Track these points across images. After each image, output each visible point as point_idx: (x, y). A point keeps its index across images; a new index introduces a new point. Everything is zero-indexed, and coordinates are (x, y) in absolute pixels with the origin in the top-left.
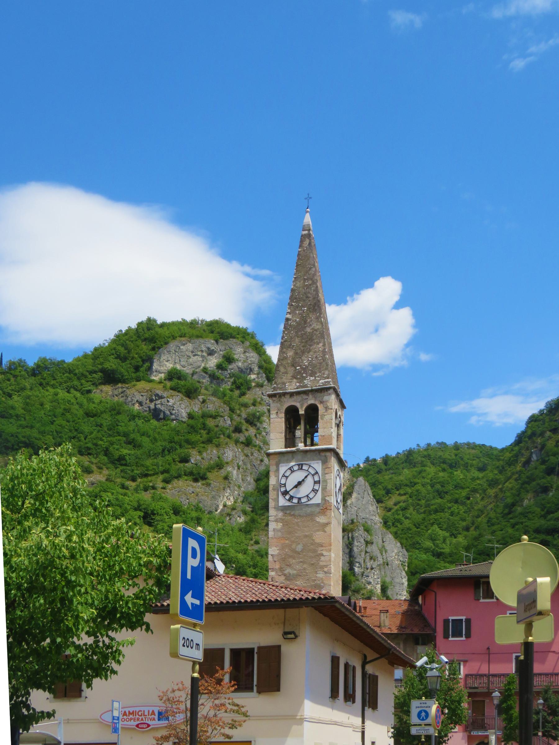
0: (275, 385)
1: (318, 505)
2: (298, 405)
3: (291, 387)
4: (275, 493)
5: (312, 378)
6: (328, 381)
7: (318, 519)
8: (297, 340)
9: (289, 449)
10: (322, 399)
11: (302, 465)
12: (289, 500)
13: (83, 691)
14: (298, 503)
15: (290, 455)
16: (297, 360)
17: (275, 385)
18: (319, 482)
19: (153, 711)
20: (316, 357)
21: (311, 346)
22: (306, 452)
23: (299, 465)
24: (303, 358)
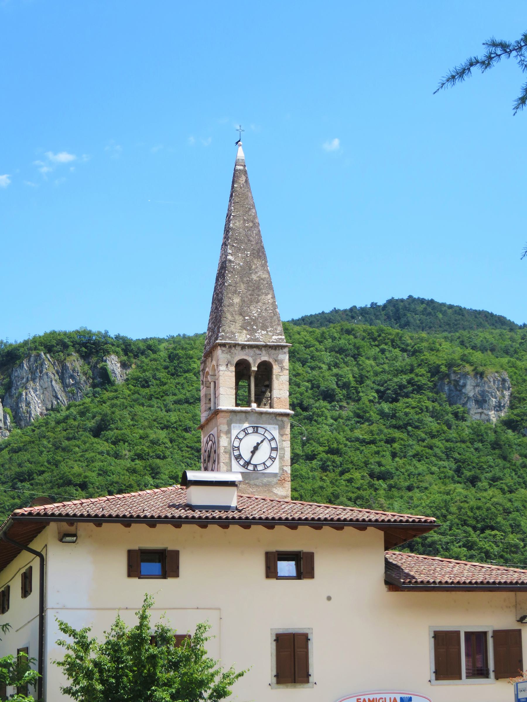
0: (223, 334)
1: (275, 475)
2: (250, 360)
3: (242, 338)
4: (227, 456)
5: (264, 332)
6: (280, 339)
7: (275, 491)
8: (243, 286)
9: (239, 408)
10: (277, 357)
11: (257, 427)
12: (243, 466)
13: (275, 676)
14: (254, 470)
15: (244, 415)
16: (246, 309)
17: (223, 334)
18: (276, 449)
19: (395, 699)
20: (266, 309)
21: (259, 295)
22: (261, 413)
24: (252, 308)
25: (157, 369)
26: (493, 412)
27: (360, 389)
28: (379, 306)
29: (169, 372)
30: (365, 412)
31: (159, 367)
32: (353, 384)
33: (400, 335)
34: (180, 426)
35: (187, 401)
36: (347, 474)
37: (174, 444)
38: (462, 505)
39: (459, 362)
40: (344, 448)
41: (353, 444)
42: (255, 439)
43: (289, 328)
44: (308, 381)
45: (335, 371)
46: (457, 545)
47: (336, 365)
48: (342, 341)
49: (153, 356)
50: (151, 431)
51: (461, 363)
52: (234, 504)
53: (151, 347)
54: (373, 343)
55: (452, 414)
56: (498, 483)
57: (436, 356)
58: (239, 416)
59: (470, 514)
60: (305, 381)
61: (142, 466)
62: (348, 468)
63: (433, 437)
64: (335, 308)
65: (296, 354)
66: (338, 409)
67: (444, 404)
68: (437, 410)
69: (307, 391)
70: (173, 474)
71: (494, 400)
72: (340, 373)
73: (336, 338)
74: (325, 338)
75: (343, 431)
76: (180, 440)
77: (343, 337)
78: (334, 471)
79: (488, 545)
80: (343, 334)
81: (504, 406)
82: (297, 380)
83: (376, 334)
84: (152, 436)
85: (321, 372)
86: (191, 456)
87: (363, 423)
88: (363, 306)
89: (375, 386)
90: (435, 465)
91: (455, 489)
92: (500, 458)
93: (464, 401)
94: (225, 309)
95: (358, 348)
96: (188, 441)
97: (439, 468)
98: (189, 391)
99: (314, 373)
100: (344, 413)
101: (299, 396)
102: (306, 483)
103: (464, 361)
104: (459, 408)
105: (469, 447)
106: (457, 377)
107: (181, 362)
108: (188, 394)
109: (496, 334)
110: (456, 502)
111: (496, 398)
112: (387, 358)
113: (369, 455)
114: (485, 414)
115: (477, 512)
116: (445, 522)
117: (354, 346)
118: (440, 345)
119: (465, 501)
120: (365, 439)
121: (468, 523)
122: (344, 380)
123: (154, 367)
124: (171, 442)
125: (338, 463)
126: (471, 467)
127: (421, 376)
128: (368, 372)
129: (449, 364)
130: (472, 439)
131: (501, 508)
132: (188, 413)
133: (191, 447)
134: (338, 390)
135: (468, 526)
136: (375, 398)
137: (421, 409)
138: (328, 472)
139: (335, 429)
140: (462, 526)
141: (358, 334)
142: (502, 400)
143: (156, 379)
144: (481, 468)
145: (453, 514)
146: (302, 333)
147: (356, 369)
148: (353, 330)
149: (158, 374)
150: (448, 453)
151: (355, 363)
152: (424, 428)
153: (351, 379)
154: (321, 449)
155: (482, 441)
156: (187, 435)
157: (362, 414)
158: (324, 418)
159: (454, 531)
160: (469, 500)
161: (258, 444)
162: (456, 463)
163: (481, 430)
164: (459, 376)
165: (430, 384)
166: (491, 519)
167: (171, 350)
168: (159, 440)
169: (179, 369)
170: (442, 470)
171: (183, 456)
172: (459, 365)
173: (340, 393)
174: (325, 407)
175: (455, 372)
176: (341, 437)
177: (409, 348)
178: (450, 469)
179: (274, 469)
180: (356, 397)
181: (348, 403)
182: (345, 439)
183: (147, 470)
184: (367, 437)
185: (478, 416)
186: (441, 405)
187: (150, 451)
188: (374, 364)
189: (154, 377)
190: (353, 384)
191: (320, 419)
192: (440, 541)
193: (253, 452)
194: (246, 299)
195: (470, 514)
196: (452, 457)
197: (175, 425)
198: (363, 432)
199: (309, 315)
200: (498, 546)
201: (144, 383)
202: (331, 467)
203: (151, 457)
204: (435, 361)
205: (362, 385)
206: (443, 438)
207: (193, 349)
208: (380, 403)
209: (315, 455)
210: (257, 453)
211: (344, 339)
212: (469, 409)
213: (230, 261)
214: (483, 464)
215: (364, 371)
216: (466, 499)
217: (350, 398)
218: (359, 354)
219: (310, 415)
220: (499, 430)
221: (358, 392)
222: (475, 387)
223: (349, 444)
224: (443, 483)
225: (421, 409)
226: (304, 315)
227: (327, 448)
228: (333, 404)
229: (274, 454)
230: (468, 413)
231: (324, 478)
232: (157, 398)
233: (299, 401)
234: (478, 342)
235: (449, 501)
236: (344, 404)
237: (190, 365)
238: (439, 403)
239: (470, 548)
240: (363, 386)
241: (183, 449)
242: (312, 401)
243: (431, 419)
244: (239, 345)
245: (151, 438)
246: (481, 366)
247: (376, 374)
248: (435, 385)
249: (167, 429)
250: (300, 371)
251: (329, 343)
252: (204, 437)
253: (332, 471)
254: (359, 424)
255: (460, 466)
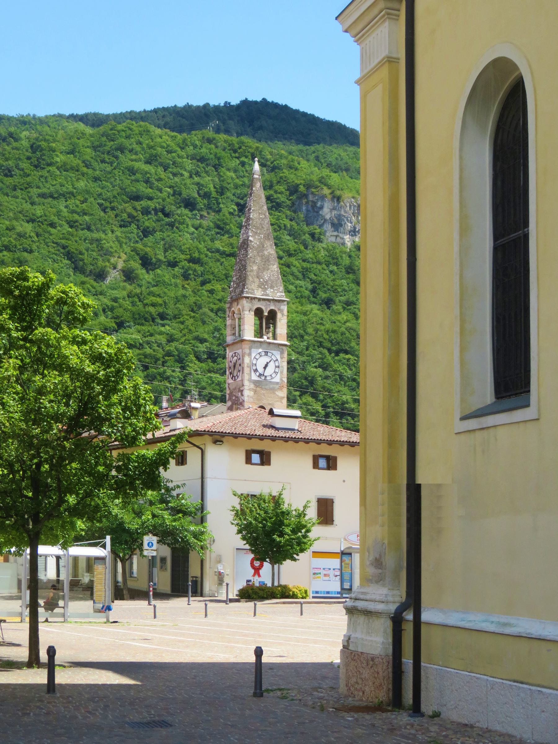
1: (277, 383)
2: (264, 308)
3: (259, 294)
12: (259, 376)
15: (259, 343)
18: (278, 367)
21: (269, 265)
22: (270, 343)
23: (265, 352)
24: (264, 273)
25: (20, 159)
26: (348, 236)
27: (220, 200)
28: (233, 106)
29: (32, 163)
30: (226, 224)
31: (22, 157)
32: (214, 194)
33: (260, 149)
34: (46, 220)
35: (51, 196)
36: (208, 285)
37: (40, 238)
38: (318, 326)
39: (318, 183)
40: (205, 258)
41: (213, 254)
42: (266, 359)
43: (151, 130)
44: (170, 187)
45: (196, 179)
46: (314, 365)
47: (197, 174)
48: (204, 150)
49: (15, 144)
50: (17, 224)
51: (319, 185)
52: (296, 428)
53: (12, 134)
54: (233, 155)
55: (309, 234)
56: (352, 307)
57: (295, 174)
58: (256, 344)
59: (326, 336)
60: (167, 187)
61: (9, 257)
62: (209, 279)
63: (290, 255)
64: (188, 103)
65: (158, 158)
66: (198, 218)
67: (301, 224)
68: (294, 229)
69: (169, 197)
70: (41, 269)
71: (349, 224)
72: (202, 182)
73: (197, 145)
74: (187, 145)
75: (204, 242)
76: (47, 235)
77: (204, 145)
78: (195, 280)
79: (342, 367)
80: (204, 143)
81: (358, 232)
82: (159, 185)
83: (237, 146)
84: (19, 229)
85: (183, 180)
86: (57, 252)
87: (223, 235)
88: (217, 104)
89: (235, 199)
90: (292, 284)
91: (312, 310)
92: (353, 283)
93: (320, 222)
94: (248, 273)
95: (219, 159)
96: (54, 236)
97: (296, 287)
98: (53, 185)
99: (176, 179)
100: (205, 223)
101: (161, 201)
102: (169, 290)
103: (322, 183)
104: (316, 229)
105: (325, 269)
106: (315, 198)
107: (44, 155)
108: (52, 189)
109: (350, 151)
110: (313, 323)
111: (351, 223)
112: (246, 171)
113: (229, 268)
114: (341, 238)
115: (333, 335)
116: (302, 342)
117: (215, 155)
118: (299, 164)
119: (321, 324)
120: (225, 251)
121: (324, 344)
122: (206, 190)
123: (17, 156)
124: (37, 236)
125: (200, 273)
126: (325, 289)
127: (280, 193)
128: (229, 184)
129: (307, 185)
130: (328, 261)
131: (355, 334)
132: (52, 208)
133: (56, 243)
134: (199, 199)
135: (324, 348)
136: (235, 210)
137: (279, 227)
138: (189, 281)
139: (196, 237)
140: (319, 347)
141: (219, 144)
142: (357, 226)
143: (18, 169)
144: (335, 291)
145: (310, 335)
146: (164, 137)
147: (217, 179)
148: (214, 139)
149: (20, 164)
150: (305, 273)
151: (216, 173)
152: (282, 246)
153: (212, 189)
154: (183, 257)
155: (337, 264)
156: (53, 231)
157: (222, 226)
158: (185, 226)
159: (311, 352)
160: (325, 323)
161: (267, 363)
162: (312, 284)
163: (336, 253)
164: (317, 198)
165: (289, 203)
166: (345, 343)
167: (33, 141)
168: (26, 233)
169: (42, 162)
170: (299, 289)
171: (49, 252)
172: (316, 187)
173: (201, 203)
174: (186, 215)
175: (312, 193)
176: (201, 246)
177: (269, 163)
178: (306, 289)
179: (277, 379)
180: (217, 207)
181: (208, 213)
182: (205, 249)
183: (15, 263)
184: (227, 250)
185: (333, 239)
186: (298, 224)
187: (17, 243)
188: (234, 176)
189: (17, 166)
190: (214, 194)
191: (181, 227)
192: (298, 360)
193: (265, 368)
194: (261, 268)
195: (326, 336)
196: (309, 278)
197: (40, 219)
198: (223, 244)
199: (161, 107)
200: (351, 370)
201: (7, 171)
202: (192, 276)
203: (19, 249)
204: (294, 180)
205: (223, 197)
206: (300, 258)
207: (55, 142)
208: (240, 217)
209: (176, 262)
210: (267, 368)
211: (206, 148)
212: (326, 231)
213: (251, 241)
214: (337, 287)
215: (225, 182)
216: (321, 321)
217: (211, 208)
218: (220, 165)
219: (172, 222)
220: (353, 254)
221: (218, 204)
222: (331, 210)
223: (210, 254)
224: (299, 302)
225: (279, 227)
226: (156, 107)
227: (188, 256)
228: (194, 212)
229: (277, 370)
230: (324, 235)
231: (186, 286)
232: (21, 189)
233: (161, 207)
234: (332, 159)
235: (306, 322)
236: (205, 213)
237: (53, 158)
238: (297, 223)
239: (325, 369)
240: (224, 198)
241: (49, 244)
242: (173, 207)
243: (288, 237)
244: (257, 298)
245: (18, 231)
246: (339, 190)
247: (236, 187)
248: (293, 204)
249: (33, 223)
250: (163, 177)
251: (190, 150)
252: (229, 352)
253: (193, 279)
254: (219, 236)
255: (316, 288)
